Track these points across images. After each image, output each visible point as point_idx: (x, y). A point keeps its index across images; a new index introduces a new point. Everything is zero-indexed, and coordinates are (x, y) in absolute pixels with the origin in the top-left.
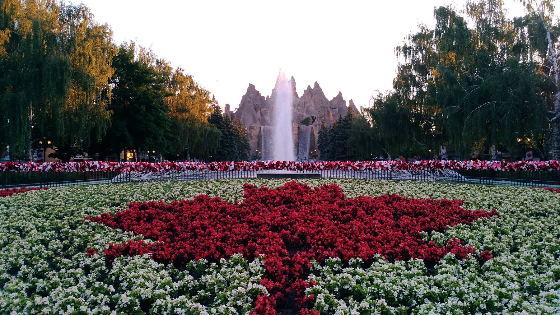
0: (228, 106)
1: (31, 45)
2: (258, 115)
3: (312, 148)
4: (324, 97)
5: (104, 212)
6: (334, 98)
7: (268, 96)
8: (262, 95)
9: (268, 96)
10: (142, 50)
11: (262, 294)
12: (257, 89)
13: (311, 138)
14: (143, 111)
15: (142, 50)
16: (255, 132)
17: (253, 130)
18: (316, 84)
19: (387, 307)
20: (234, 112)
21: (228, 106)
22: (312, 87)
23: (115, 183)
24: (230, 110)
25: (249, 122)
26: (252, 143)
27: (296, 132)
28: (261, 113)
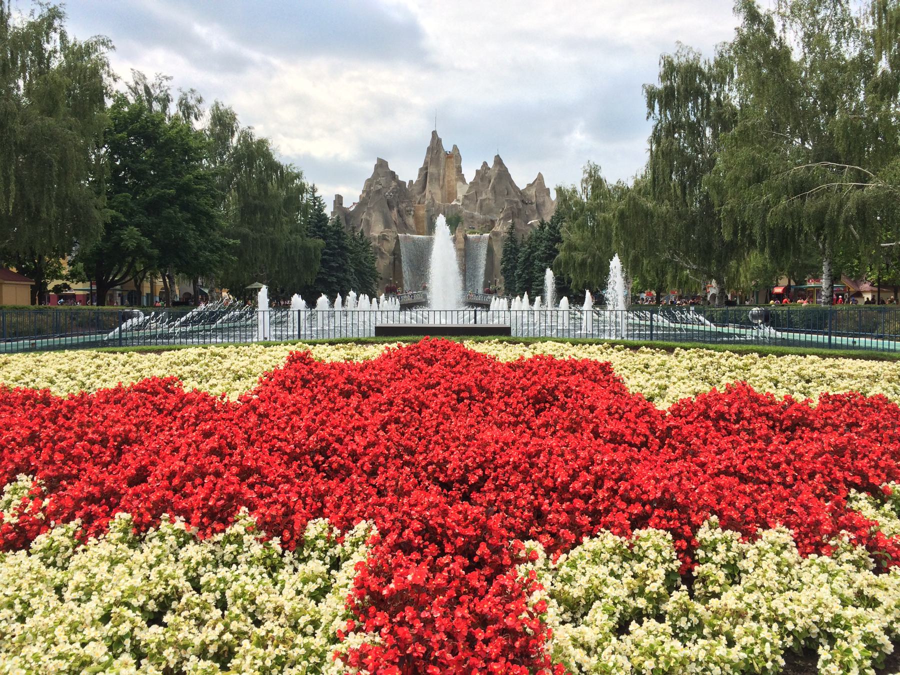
0: (339, 199)
2: (394, 214)
3: (489, 273)
4: (511, 182)
5: (6, 495)
6: (529, 186)
7: (411, 182)
8: (400, 179)
9: (411, 182)
10: (559, 191)
11: (379, 571)
12: (391, 168)
13: (488, 255)
14: (182, 215)
15: (559, 191)
16: (388, 246)
17: (385, 243)
18: (498, 161)
20: (351, 209)
21: (339, 199)
22: (491, 165)
24: (344, 206)
25: (377, 230)
26: (382, 265)
27: (462, 246)
28: (398, 211)
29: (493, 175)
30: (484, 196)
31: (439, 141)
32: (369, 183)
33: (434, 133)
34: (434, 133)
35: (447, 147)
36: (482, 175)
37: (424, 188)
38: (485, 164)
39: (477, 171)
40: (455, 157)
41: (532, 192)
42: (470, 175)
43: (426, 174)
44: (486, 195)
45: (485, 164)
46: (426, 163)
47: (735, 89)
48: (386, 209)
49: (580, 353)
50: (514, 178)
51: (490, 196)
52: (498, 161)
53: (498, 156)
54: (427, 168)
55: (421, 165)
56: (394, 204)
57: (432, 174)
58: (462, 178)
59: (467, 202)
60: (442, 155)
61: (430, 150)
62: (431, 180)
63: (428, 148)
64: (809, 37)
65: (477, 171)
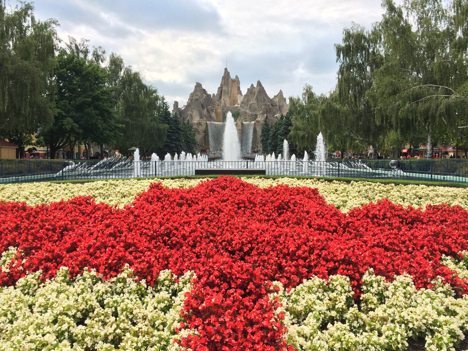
0: (176, 104)
1: (65, 140)
2: (205, 111)
3: (254, 142)
4: (266, 95)
5: (3, 257)
6: (275, 96)
7: (214, 95)
8: (208, 93)
9: (214, 95)
12: (204, 87)
13: (254, 132)
14: (95, 112)
16: (202, 128)
17: (200, 126)
18: (259, 84)
19: (34, 146)
20: (183, 109)
21: (176, 104)
22: (255, 86)
23: (115, 171)
24: (179, 107)
25: (196, 119)
26: (199, 138)
27: (240, 128)
28: (207, 110)
29: (256, 91)
30: (252, 102)
31: (228, 73)
32: (192, 95)
33: (226, 69)
34: (226, 69)
35: (233, 76)
36: (251, 91)
37: (221, 98)
38: (252, 85)
39: (248, 89)
40: (236, 81)
41: (277, 100)
42: (244, 91)
43: (222, 91)
44: (253, 101)
45: (252, 85)
46: (221, 85)
47: (382, 47)
48: (201, 109)
49: (302, 184)
50: (267, 92)
51: (255, 102)
52: (259, 84)
53: (259, 81)
54: (222, 88)
55: (219, 86)
56: (205, 106)
57: (225, 91)
58: (240, 93)
59: (243, 105)
60: (230, 81)
61: (223, 78)
62: (224, 93)
63: (223, 77)
64: (421, 19)
65: (248, 89)
